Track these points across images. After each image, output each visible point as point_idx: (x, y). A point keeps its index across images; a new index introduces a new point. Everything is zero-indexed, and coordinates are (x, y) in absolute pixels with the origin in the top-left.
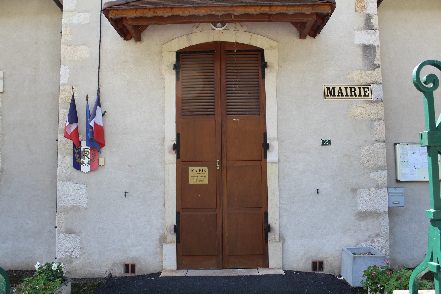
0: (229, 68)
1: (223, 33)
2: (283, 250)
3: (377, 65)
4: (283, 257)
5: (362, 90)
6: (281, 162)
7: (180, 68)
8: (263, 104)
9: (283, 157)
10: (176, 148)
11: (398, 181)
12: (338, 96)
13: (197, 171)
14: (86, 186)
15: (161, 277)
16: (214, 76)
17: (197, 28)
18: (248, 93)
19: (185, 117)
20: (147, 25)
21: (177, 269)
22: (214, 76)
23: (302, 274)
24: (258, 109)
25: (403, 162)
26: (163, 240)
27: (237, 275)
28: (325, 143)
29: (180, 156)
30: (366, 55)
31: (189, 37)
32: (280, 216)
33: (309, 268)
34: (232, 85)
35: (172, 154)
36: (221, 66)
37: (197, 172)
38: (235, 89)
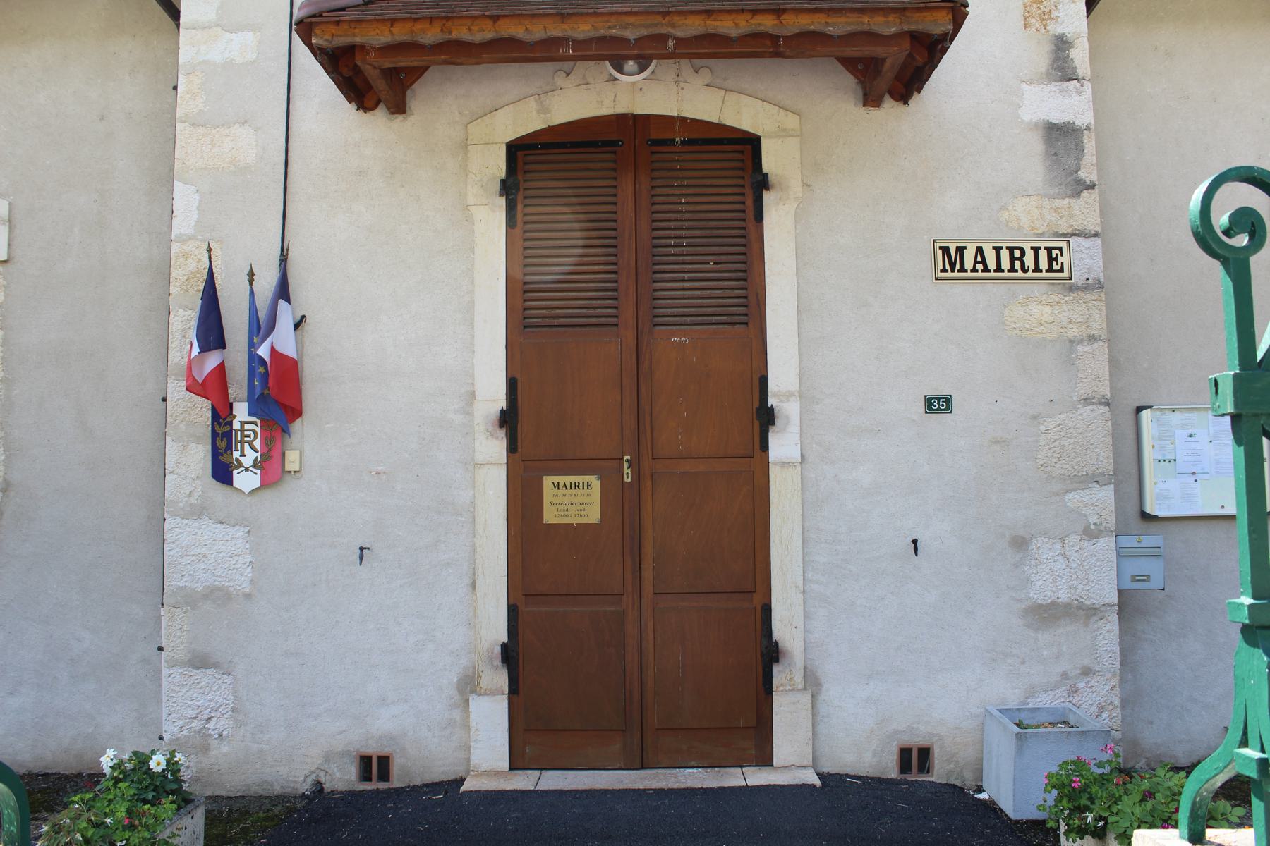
0: (658, 191)
1: (641, 89)
2: (815, 714)
3: (1085, 182)
4: (814, 734)
5: (1043, 255)
6: (810, 460)
7: (518, 190)
8: (757, 295)
9: (814, 446)
10: (508, 419)
11: (1145, 516)
12: (974, 270)
13: (566, 489)
14: (249, 532)
15: (464, 792)
16: (615, 212)
17: (568, 75)
18: (715, 263)
19: (533, 332)
20: (422, 67)
21: (511, 769)
22: (615, 212)
23: (869, 784)
24: (745, 308)
25: (1162, 461)
26: (469, 686)
27: (683, 786)
28: (935, 406)
29: (519, 444)
30: (1055, 154)
31: (544, 103)
32: (807, 616)
33: (890, 765)
34: (668, 241)
35: (497, 438)
36: (637, 186)
37: (569, 491)
38: (678, 250)
